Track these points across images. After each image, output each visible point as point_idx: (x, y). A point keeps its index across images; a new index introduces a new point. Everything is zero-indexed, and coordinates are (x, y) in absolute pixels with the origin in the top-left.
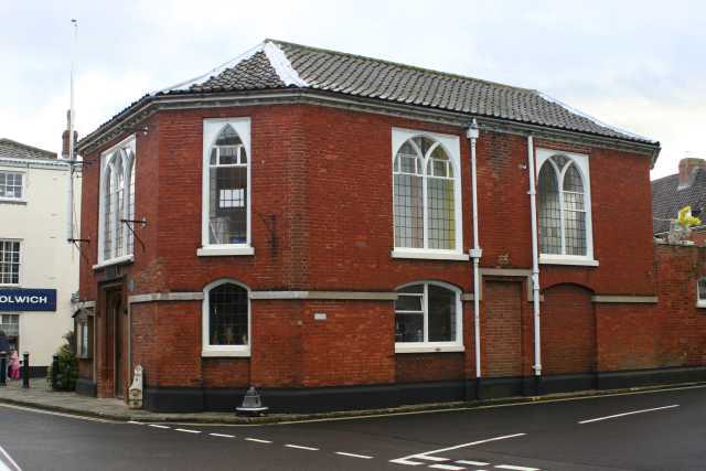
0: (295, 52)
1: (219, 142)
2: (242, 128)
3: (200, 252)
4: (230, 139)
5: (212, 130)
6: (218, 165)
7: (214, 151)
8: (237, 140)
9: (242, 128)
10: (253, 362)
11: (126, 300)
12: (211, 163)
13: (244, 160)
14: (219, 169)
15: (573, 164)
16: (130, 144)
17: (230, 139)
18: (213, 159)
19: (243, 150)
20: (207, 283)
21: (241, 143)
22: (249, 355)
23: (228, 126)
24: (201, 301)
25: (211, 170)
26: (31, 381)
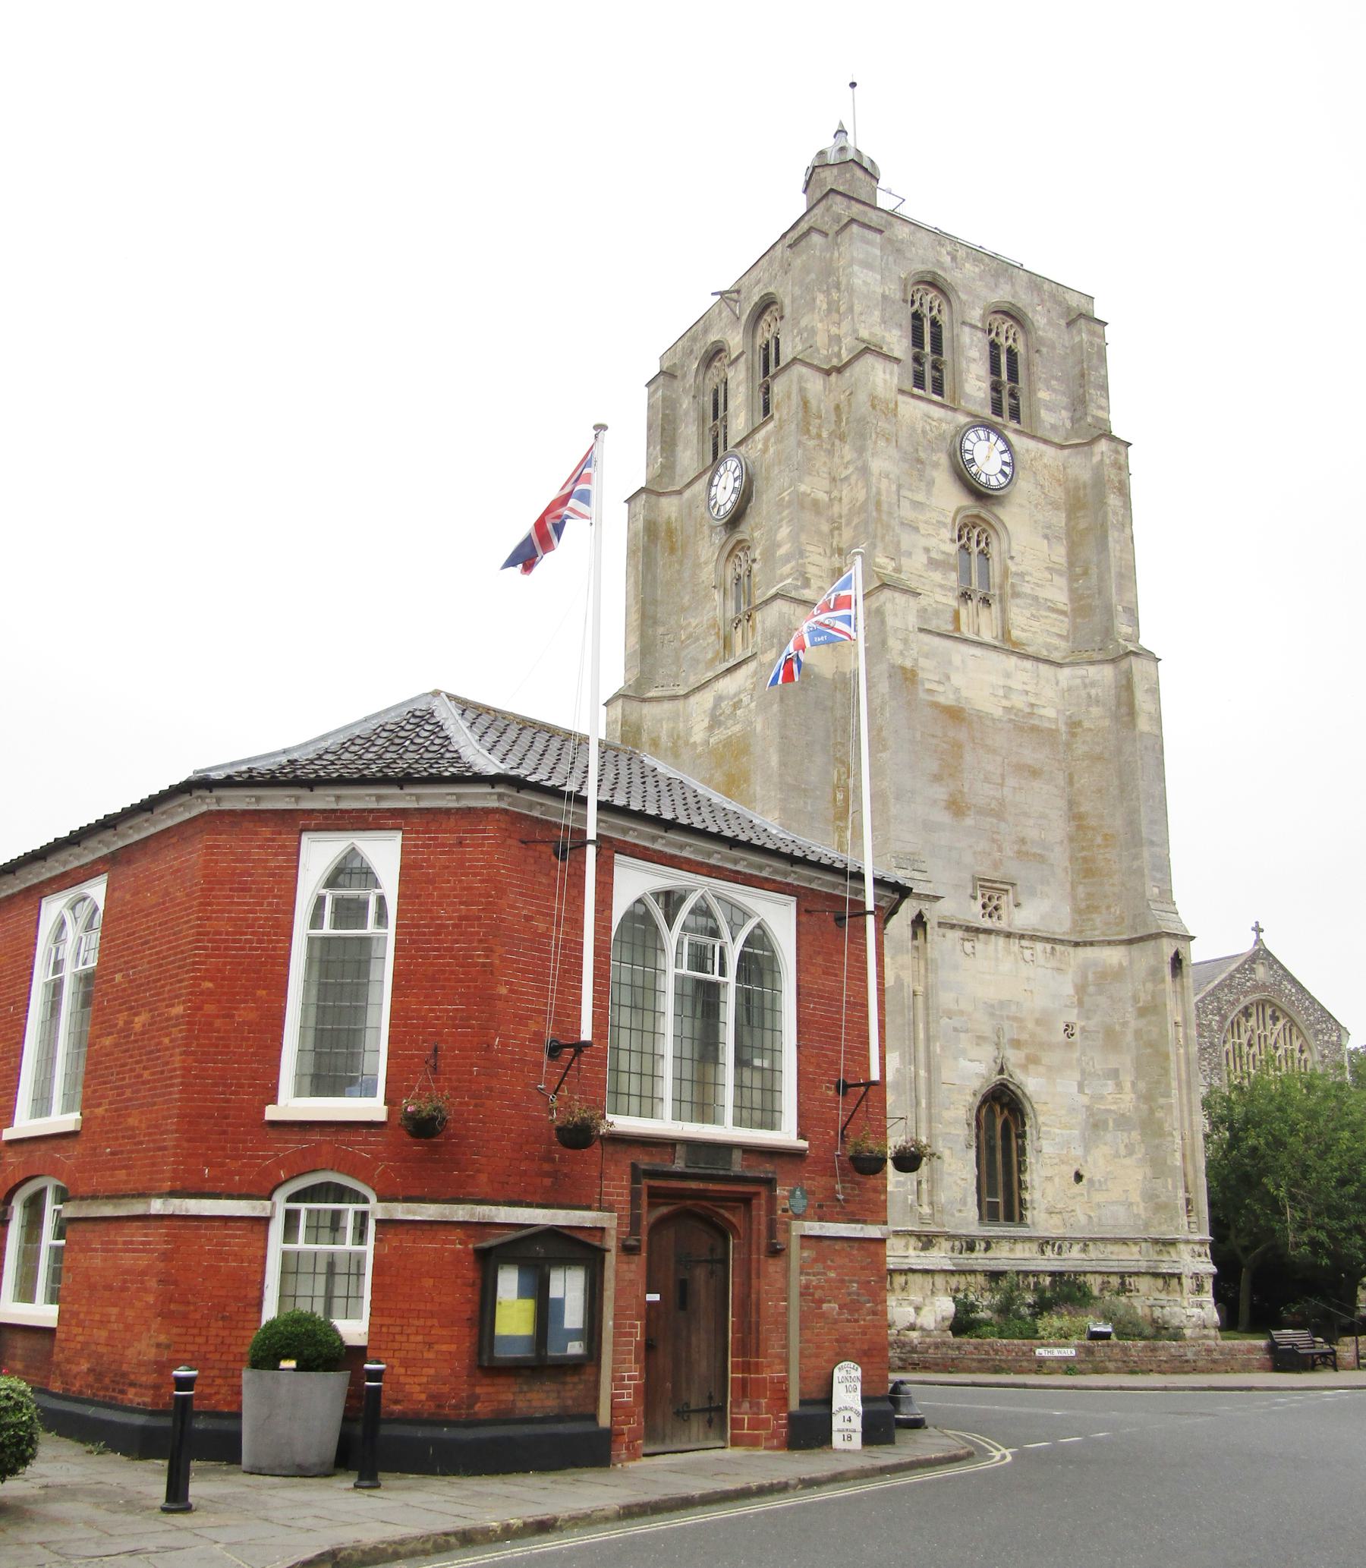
0: (473, 711)
1: (331, 882)
2: (383, 853)
3: (271, 1113)
4: (349, 871)
5: (318, 855)
6: (327, 930)
7: (320, 901)
8: (367, 877)
9: (383, 853)
10: (59, 1335)
11: (788, 1231)
12: (312, 927)
13: (381, 918)
14: (327, 940)
15: (759, 926)
16: (97, 890)
17: (349, 871)
18: (316, 921)
19: (381, 900)
20: (280, 1184)
21: (377, 885)
22: (53, 1324)
23: (353, 852)
24: (265, 1221)
25: (311, 940)
26: (198, 1489)
